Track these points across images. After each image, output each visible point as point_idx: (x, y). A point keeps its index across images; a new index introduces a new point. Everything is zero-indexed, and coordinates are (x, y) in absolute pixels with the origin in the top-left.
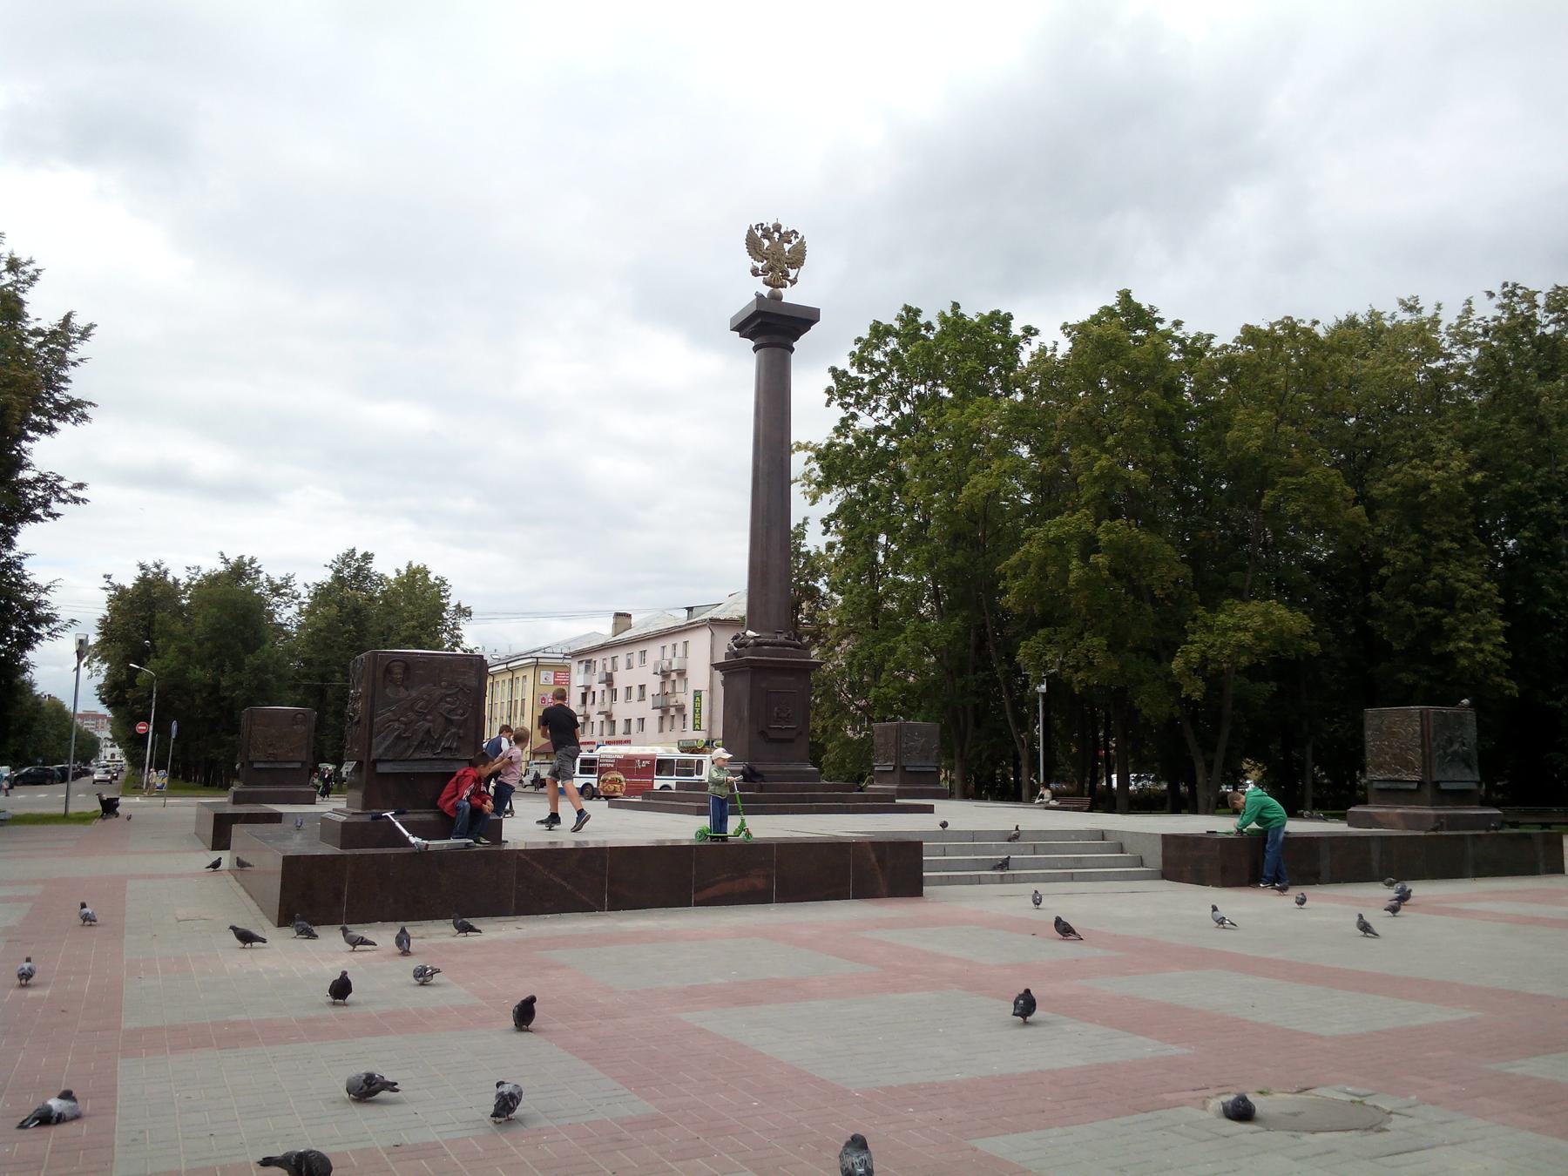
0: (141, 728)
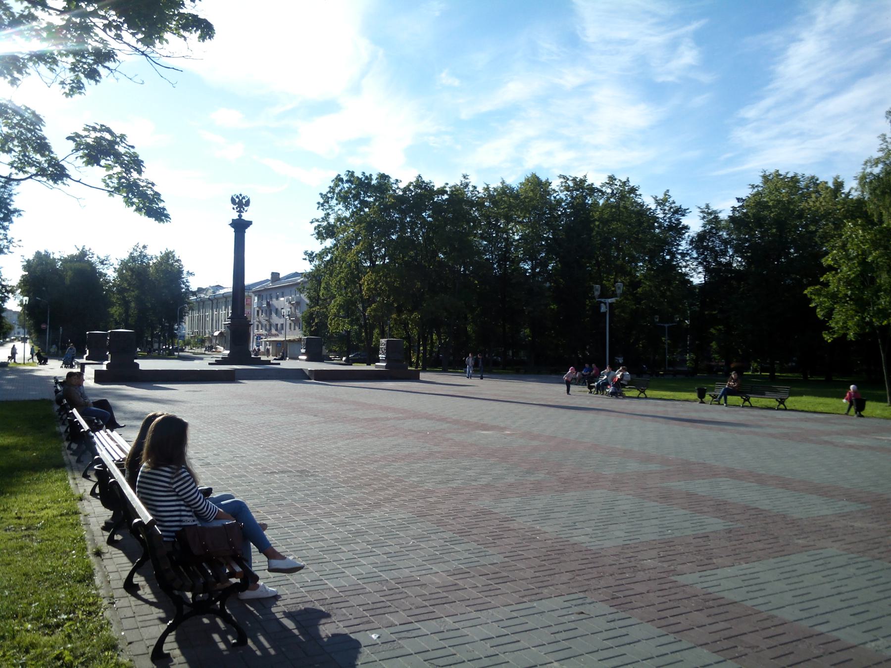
0: (43, 326)
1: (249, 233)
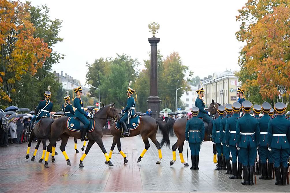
1: (159, 46)
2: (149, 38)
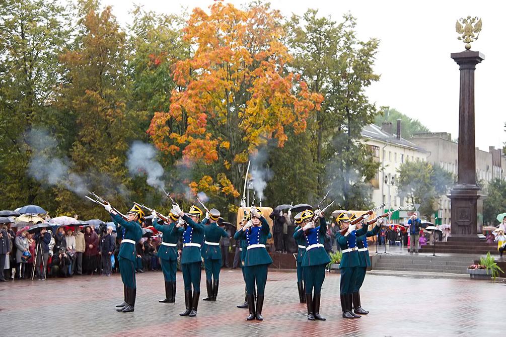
2: (451, 54)
